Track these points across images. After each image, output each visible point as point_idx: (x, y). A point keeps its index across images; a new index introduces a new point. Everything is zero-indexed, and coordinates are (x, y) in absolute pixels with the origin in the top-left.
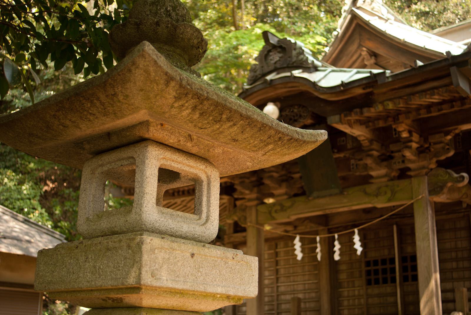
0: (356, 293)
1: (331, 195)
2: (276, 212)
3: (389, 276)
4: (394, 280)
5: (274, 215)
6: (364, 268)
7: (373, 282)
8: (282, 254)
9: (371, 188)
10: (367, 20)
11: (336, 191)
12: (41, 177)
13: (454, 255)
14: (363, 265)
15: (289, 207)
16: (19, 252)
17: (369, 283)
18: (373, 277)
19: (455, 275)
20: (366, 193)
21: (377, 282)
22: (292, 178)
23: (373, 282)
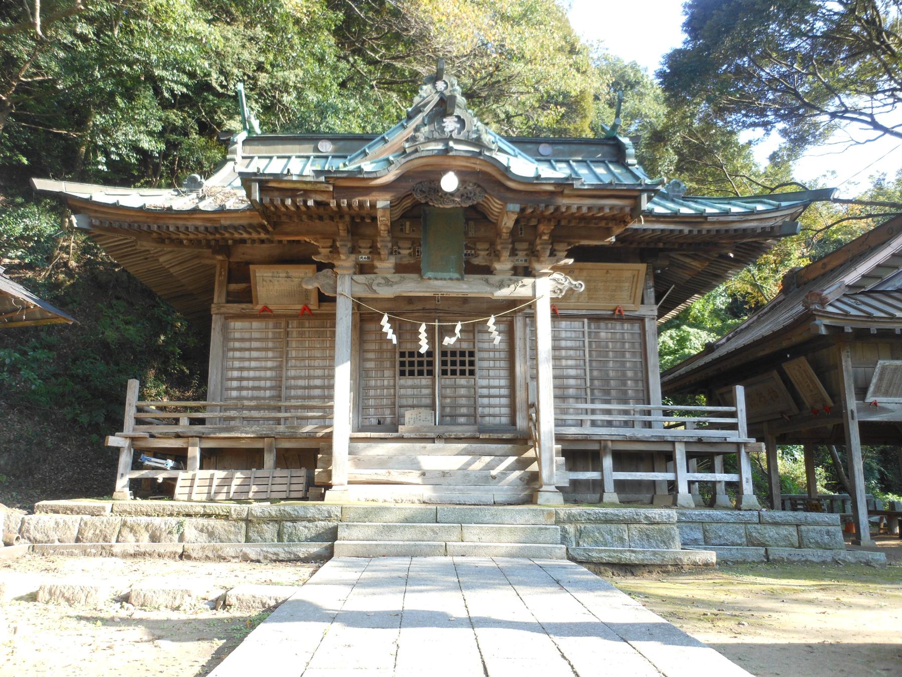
0: (386, 383)
1: (451, 279)
2: (378, 284)
3: (425, 368)
4: (431, 373)
5: (375, 288)
6: (398, 359)
7: (407, 373)
8: (295, 335)
9: (493, 279)
10: (86, 196)
11: (456, 275)
12: (231, 148)
13: (492, 354)
14: (397, 355)
15: (396, 283)
16: (692, 212)
17: (402, 373)
18: (407, 368)
19: (492, 373)
20: (487, 281)
21: (412, 373)
22: (399, 253)
23: (407, 373)
